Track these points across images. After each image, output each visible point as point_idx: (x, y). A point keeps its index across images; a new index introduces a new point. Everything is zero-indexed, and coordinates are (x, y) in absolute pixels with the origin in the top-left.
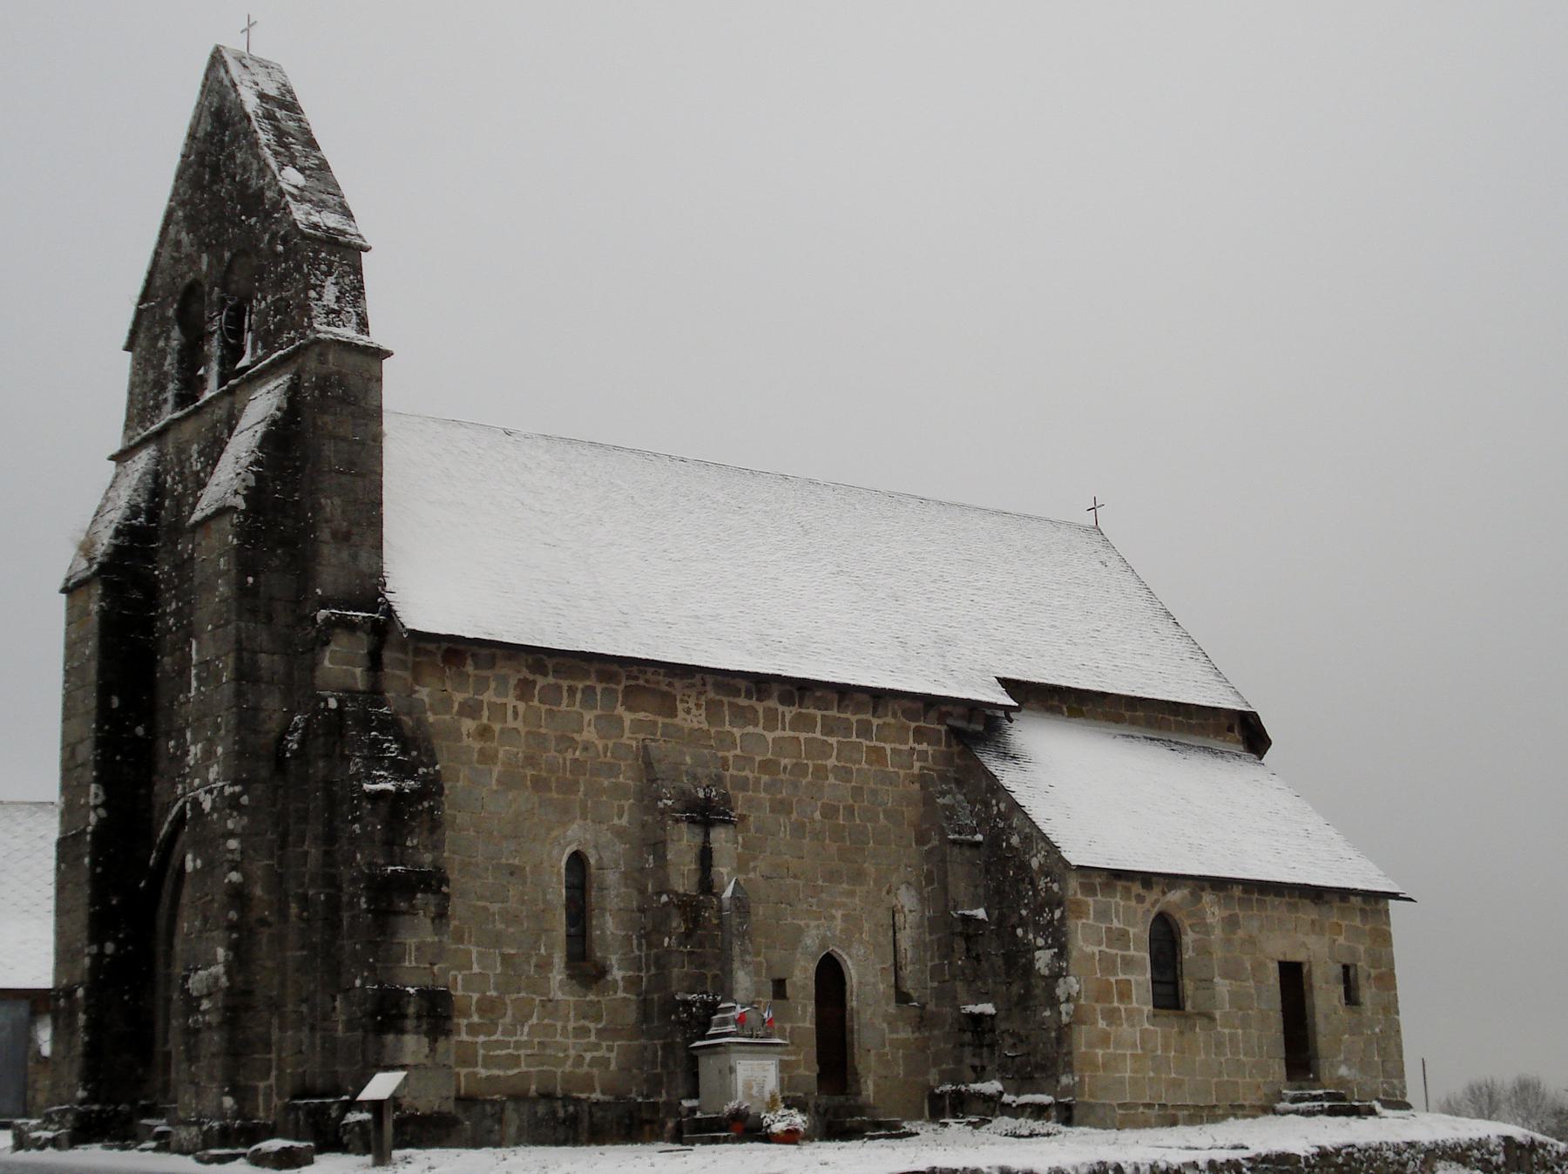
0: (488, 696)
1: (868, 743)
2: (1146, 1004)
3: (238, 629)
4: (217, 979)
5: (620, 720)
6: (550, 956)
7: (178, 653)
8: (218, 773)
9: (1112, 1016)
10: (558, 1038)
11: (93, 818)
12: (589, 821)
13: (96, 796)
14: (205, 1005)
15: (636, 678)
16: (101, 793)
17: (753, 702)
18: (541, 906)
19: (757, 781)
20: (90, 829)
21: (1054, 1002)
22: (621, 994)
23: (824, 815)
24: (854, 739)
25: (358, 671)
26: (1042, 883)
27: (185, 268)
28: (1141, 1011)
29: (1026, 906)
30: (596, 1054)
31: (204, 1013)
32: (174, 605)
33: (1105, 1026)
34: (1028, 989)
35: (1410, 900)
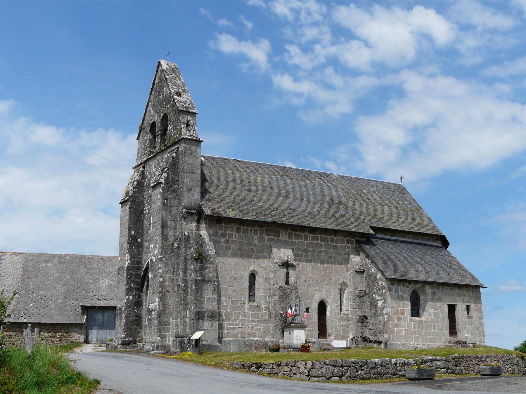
0: (228, 232)
1: (333, 244)
3: (162, 214)
5: (264, 238)
9: (399, 319)
10: (246, 323)
11: (127, 263)
12: (255, 265)
13: (128, 257)
14: (153, 313)
16: (129, 256)
17: (301, 233)
19: (302, 254)
20: (126, 266)
21: (383, 315)
22: (264, 311)
26: (380, 282)
28: (407, 318)
33: (397, 322)
34: (376, 311)
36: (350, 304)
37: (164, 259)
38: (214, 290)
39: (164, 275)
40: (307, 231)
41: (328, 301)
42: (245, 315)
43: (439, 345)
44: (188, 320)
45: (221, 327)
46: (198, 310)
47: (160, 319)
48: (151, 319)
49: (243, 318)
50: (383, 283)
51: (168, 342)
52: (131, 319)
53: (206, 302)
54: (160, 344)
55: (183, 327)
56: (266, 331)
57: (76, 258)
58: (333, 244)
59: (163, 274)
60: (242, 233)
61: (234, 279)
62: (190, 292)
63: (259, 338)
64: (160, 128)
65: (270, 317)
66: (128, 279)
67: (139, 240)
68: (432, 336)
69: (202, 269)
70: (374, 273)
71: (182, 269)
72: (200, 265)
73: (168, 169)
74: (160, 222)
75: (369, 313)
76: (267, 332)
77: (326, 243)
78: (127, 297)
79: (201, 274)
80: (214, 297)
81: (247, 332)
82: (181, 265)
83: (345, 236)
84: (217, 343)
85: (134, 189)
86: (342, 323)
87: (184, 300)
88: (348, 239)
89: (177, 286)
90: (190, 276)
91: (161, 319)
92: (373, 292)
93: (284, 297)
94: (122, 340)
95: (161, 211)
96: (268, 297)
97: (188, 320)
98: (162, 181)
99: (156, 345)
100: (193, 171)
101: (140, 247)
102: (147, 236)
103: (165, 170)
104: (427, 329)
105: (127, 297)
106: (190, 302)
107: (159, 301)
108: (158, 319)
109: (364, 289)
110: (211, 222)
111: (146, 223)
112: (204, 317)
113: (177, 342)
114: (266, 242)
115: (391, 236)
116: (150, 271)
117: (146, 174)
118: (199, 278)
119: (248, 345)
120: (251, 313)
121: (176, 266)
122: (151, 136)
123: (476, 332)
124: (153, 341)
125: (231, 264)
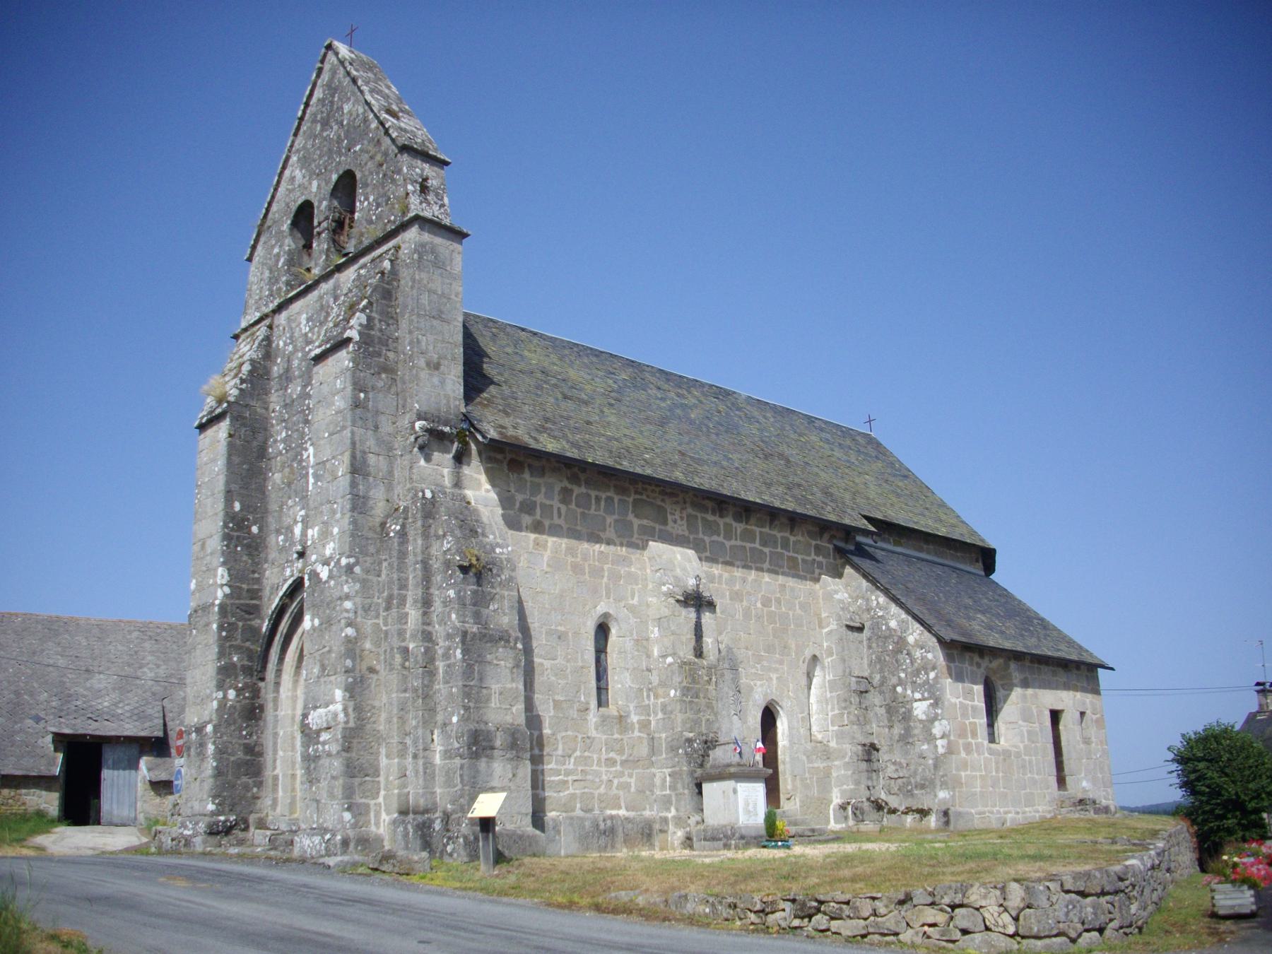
0: (540, 499)
3: (353, 433)
4: (336, 715)
5: (631, 523)
6: (588, 703)
7: (287, 470)
8: (334, 549)
10: (595, 768)
11: (220, 594)
12: (611, 600)
13: (223, 576)
14: (324, 736)
15: (641, 494)
16: (226, 575)
17: (717, 518)
18: (580, 664)
19: (721, 576)
20: (217, 602)
21: (931, 739)
22: (637, 734)
25: (446, 471)
26: (918, 654)
27: (298, 194)
28: (983, 744)
29: (904, 670)
30: (622, 780)
31: (324, 743)
32: (284, 434)
34: (908, 730)
35: (1112, 669)
36: (830, 714)
37: (357, 569)
38: (517, 666)
39: (359, 619)
40: (731, 513)
41: (784, 704)
42: (589, 742)
44: (438, 759)
45: (537, 782)
46: (472, 726)
47: (349, 755)
48: (318, 757)
49: (586, 754)
50: (930, 656)
51: (373, 828)
52: (232, 759)
53: (494, 702)
54: (351, 833)
55: (425, 780)
56: (646, 788)
57: (37, 622)
59: (356, 618)
60: (577, 506)
61: (559, 638)
62: (446, 672)
63: (627, 810)
64: (327, 213)
65: (653, 751)
66: (222, 642)
67: (255, 529)
69: (481, 600)
70: (895, 630)
71: (415, 601)
72: (475, 587)
73: (370, 303)
74: (346, 458)
75: (879, 732)
76: (648, 793)
78: (220, 695)
79: (477, 616)
80: (517, 688)
81: (596, 793)
82: (410, 587)
84: (530, 830)
85: (241, 384)
86: (816, 765)
87: (426, 697)
88: (819, 542)
89: (400, 653)
90: (442, 622)
91: (354, 754)
92: (894, 680)
93: (693, 691)
94: (207, 819)
95: (349, 423)
96: (645, 694)
97: (438, 759)
98: (353, 334)
99: (339, 837)
100: (441, 312)
101: (257, 549)
102: (280, 517)
103: (361, 306)
105: (220, 695)
106: (444, 703)
107: (344, 699)
108: (344, 754)
109: (866, 674)
110: (495, 465)
111: (278, 481)
112: (493, 748)
113: (410, 827)
114: (636, 536)
116: (309, 609)
117: (278, 345)
119: (605, 833)
121: (396, 592)
122: (292, 243)
124: (329, 825)
125: (549, 594)
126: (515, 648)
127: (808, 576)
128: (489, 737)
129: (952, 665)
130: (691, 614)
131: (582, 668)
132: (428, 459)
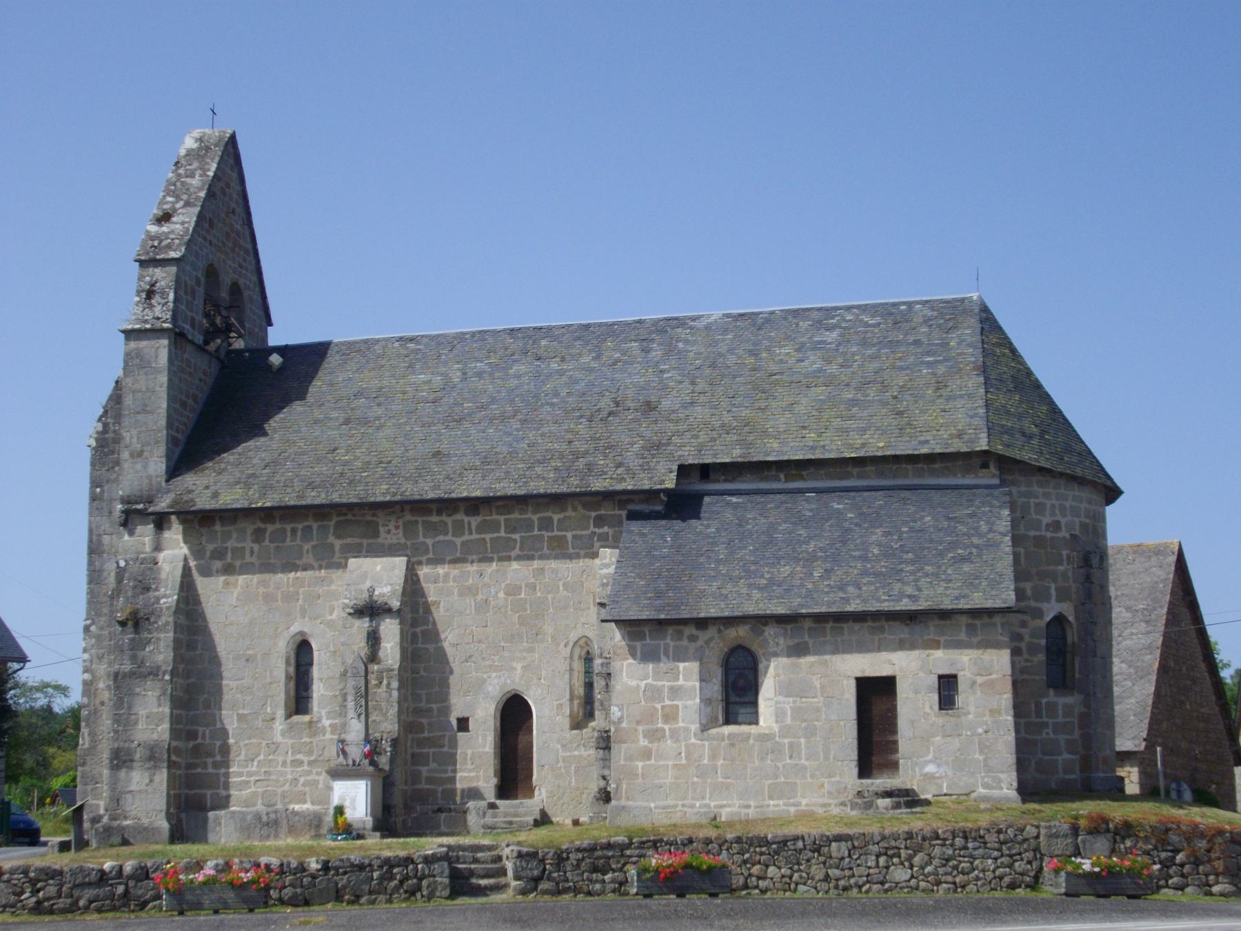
0: (231, 544)
1: (550, 534)
2: (693, 723)
5: (332, 546)
6: (274, 714)
9: (655, 735)
12: (307, 619)
17: (444, 518)
18: (269, 680)
22: (328, 736)
23: (508, 594)
24: (536, 532)
25: (147, 539)
28: (687, 730)
30: (308, 778)
33: (646, 743)
37: (93, 628)
38: (164, 694)
39: (94, 666)
40: (462, 509)
42: (274, 748)
43: (807, 805)
49: (271, 757)
58: (550, 534)
61: (247, 660)
63: (313, 803)
68: (783, 779)
77: (524, 534)
83: (588, 506)
86: (576, 753)
100: (145, 405)
104: (763, 759)
112: (132, 761)
114: (337, 554)
115: (786, 481)
118: (127, 667)
120: (292, 745)
123: (977, 756)
126: (162, 679)
127: (582, 552)
128: (130, 752)
129: (638, 644)
130: (364, 624)
131: (271, 683)
132: (131, 533)
